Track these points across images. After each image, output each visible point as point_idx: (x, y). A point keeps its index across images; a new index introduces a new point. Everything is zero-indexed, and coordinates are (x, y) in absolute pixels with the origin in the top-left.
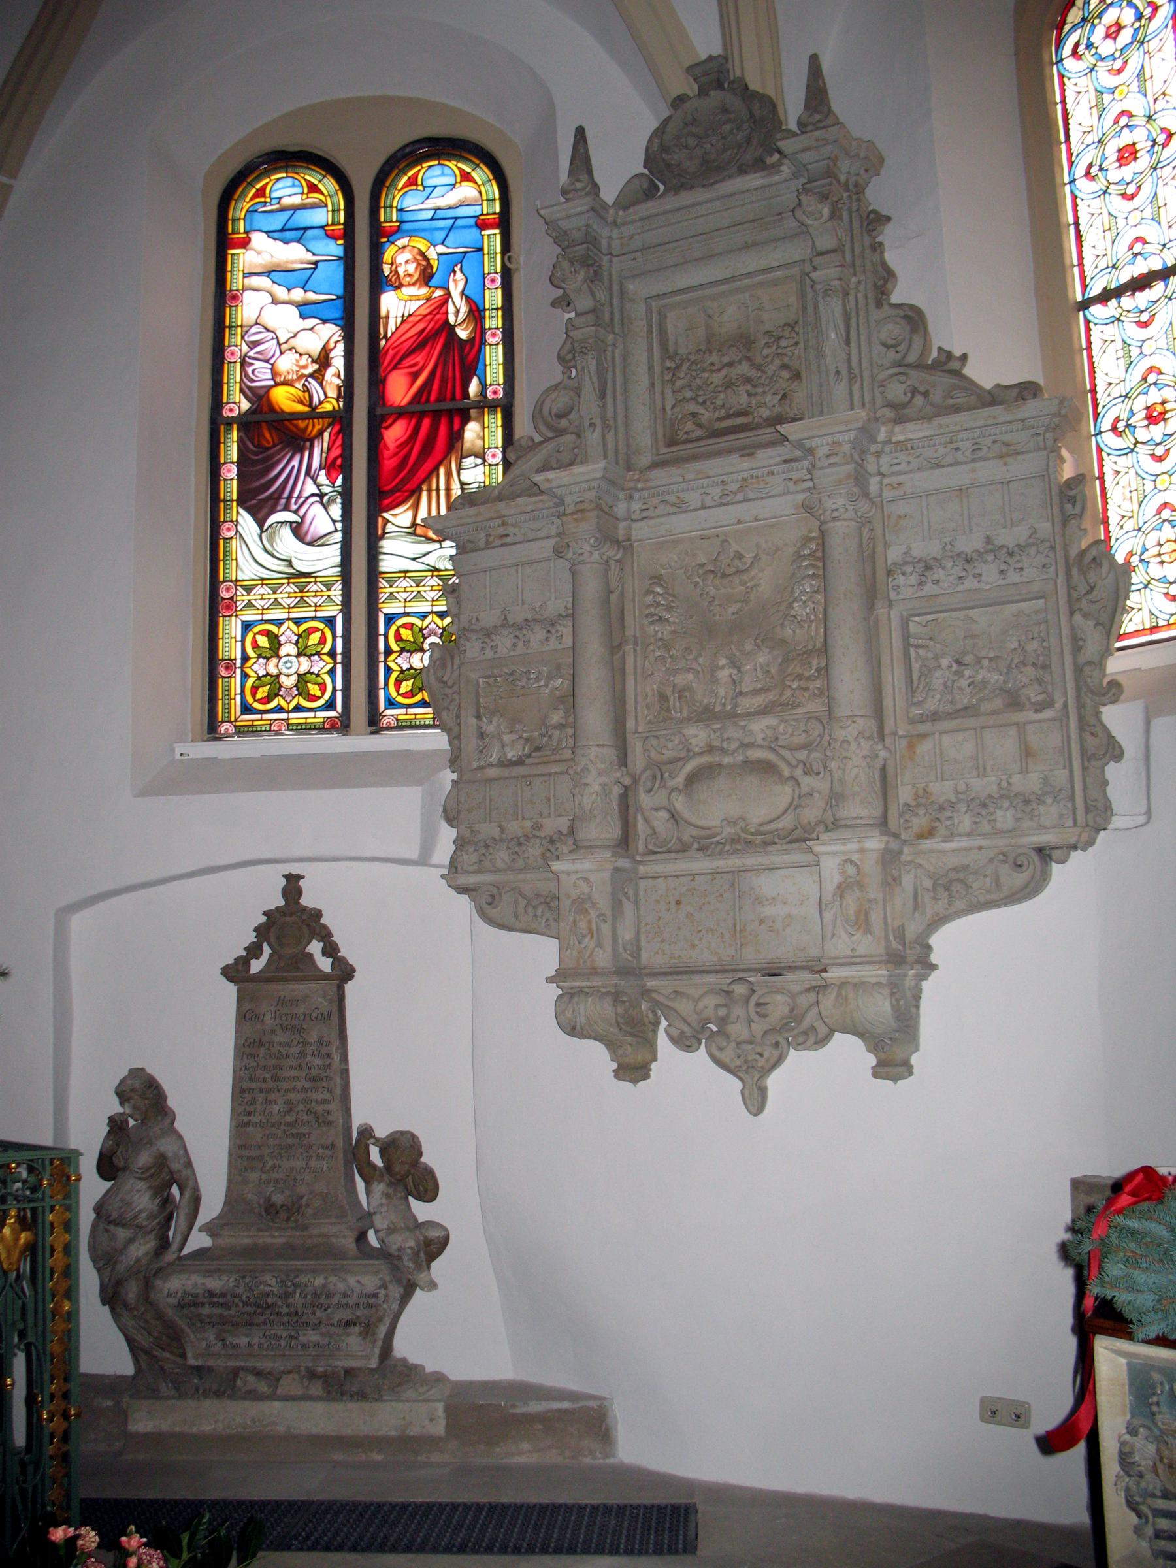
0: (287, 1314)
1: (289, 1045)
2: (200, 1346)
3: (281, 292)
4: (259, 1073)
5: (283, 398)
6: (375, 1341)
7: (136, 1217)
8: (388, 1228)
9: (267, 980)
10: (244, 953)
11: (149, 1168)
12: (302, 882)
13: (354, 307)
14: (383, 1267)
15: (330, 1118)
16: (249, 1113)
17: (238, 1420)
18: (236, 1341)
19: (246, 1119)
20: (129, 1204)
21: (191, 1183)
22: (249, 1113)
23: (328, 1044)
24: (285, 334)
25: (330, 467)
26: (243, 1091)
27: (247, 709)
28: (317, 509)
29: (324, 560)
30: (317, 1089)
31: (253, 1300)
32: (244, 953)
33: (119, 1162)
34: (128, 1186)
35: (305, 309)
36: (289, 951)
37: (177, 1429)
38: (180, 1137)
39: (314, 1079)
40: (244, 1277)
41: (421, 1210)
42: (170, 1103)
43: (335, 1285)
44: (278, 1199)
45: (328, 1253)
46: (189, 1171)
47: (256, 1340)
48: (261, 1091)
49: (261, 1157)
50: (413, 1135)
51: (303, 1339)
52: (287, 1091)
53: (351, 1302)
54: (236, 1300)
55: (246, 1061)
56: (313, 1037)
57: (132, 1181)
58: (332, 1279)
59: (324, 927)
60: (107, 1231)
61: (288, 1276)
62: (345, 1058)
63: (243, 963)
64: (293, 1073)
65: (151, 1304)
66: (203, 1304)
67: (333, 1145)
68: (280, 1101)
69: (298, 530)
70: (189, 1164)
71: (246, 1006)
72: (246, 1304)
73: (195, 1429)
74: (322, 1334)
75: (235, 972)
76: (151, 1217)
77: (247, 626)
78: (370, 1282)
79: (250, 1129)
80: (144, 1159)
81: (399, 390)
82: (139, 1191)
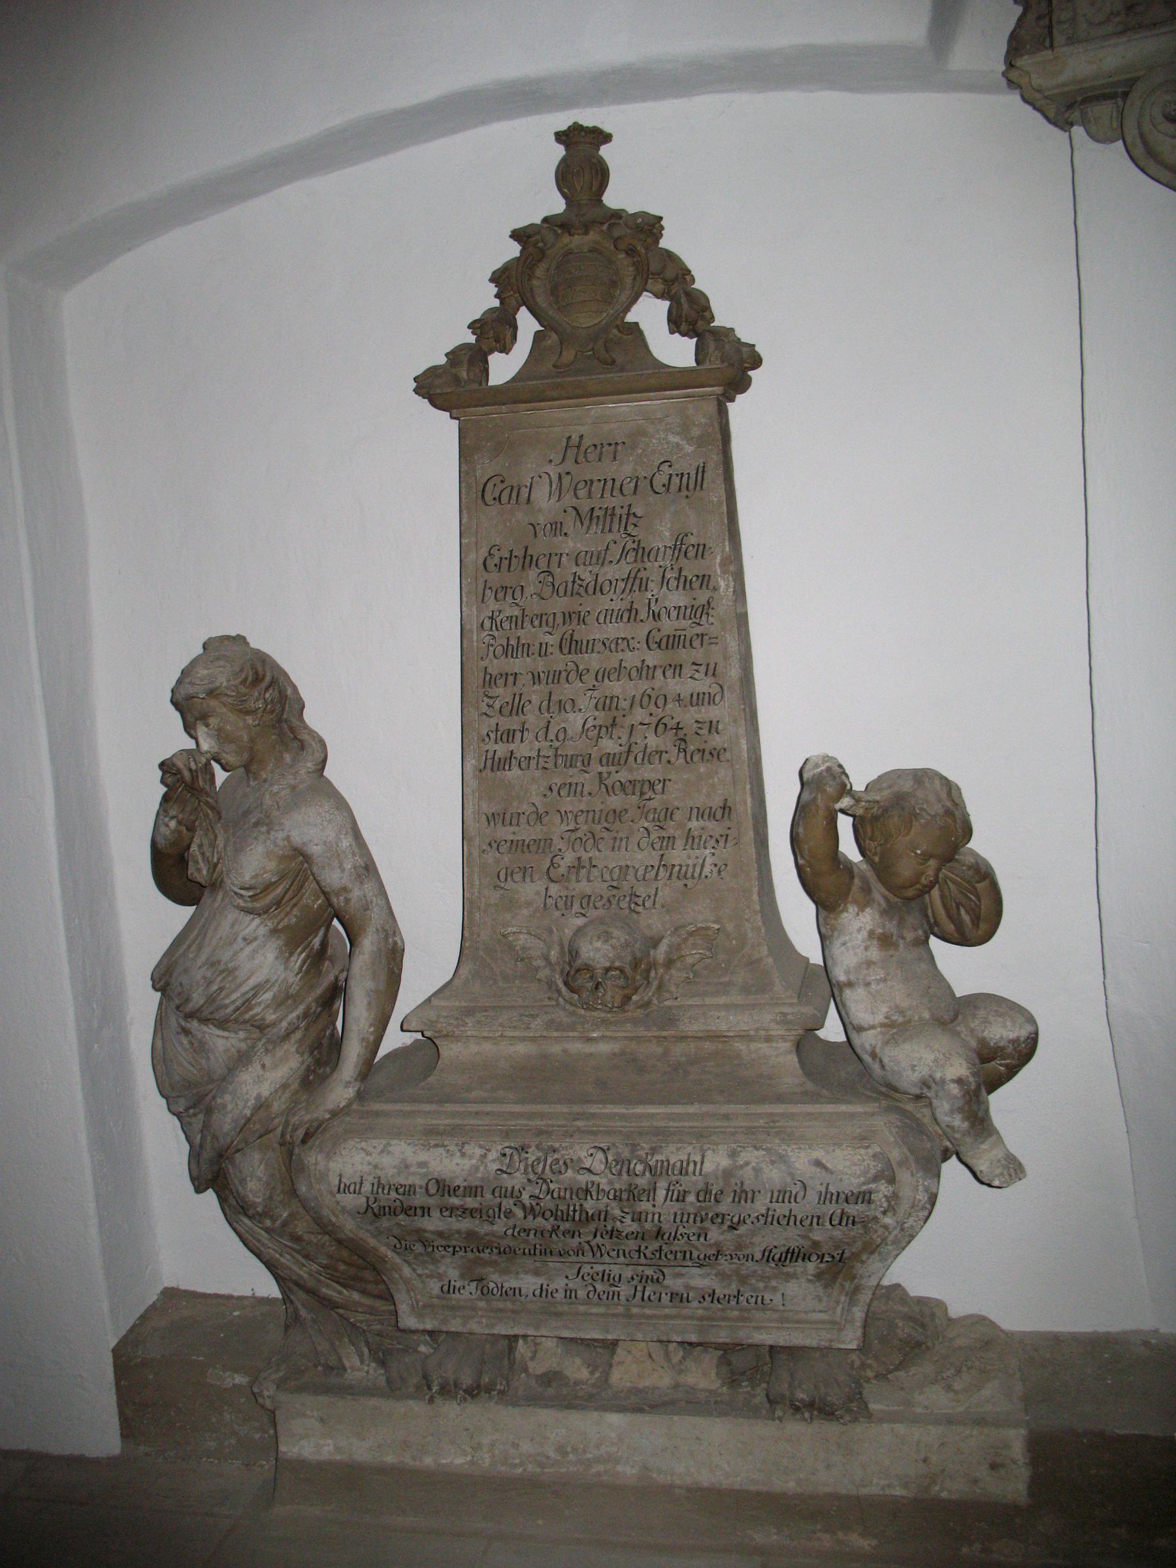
0: (636, 1236)
1: (600, 559)
2: (420, 1294)
4: (526, 634)
6: (857, 1290)
7: (247, 1004)
8: (889, 1025)
9: (536, 397)
10: (472, 339)
11: (268, 887)
12: (605, 151)
14: (879, 1122)
15: (717, 741)
16: (509, 736)
17: (526, 1447)
18: (511, 1283)
19: (501, 749)
20: (231, 972)
21: (376, 917)
22: (509, 736)
23: (701, 550)
26: (490, 680)
30: (678, 668)
31: (547, 1203)
32: (472, 339)
33: (199, 871)
34: (225, 928)
36: (585, 320)
37: (390, 1459)
38: (341, 805)
39: (672, 642)
40: (523, 1149)
41: (961, 967)
42: (312, 717)
43: (757, 1170)
44: (596, 952)
45: (725, 1079)
46: (369, 887)
47: (559, 1283)
48: (536, 678)
49: (549, 842)
50: (950, 788)
51: (673, 1283)
52: (603, 675)
53: (799, 1210)
54: (508, 1203)
55: (493, 605)
56: (662, 535)
57: (232, 915)
58: (750, 1156)
59: (670, 256)
60: (186, 1032)
61: (634, 1147)
62: (740, 593)
63: (471, 358)
64: (613, 630)
65: (304, 1204)
66: (426, 1211)
67: (726, 808)
68: (585, 702)
70: (369, 869)
71: (485, 468)
72: (530, 1211)
73: (428, 1461)
74: (723, 1276)
75: (450, 385)
76: (285, 999)
78: (848, 1166)
79: (514, 774)
80: (254, 862)
82: (248, 941)
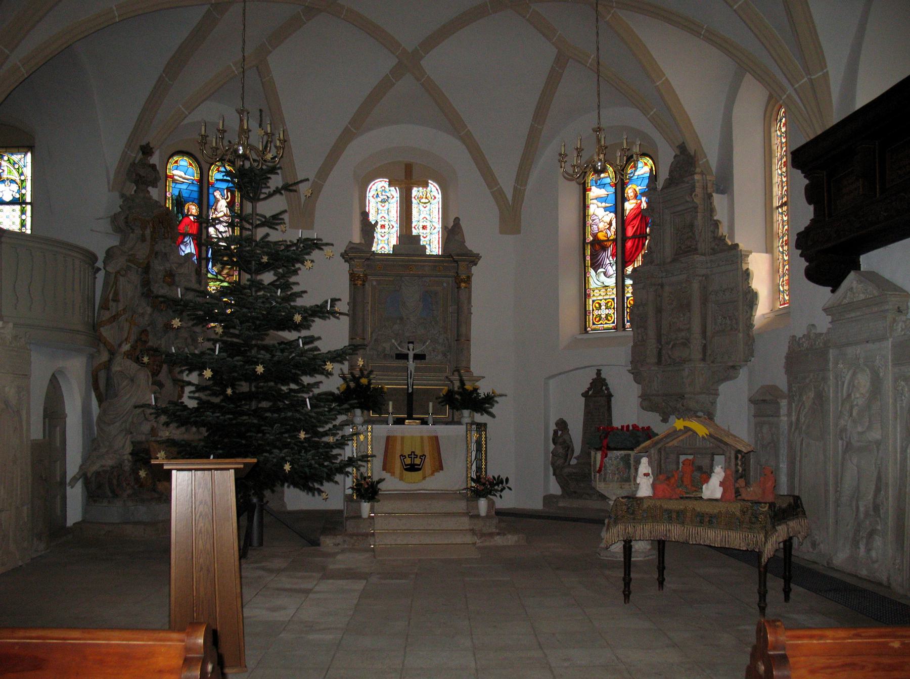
3: (599, 204)
5: (601, 236)
13: (618, 208)
24: (601, 218)
25: (612, 255)
27: (594, 324)
28: (610, 267)
29: (611, 282)
35: (606, 209)
63: (587, 392)
69: (605, 274)
75: (585, 395)
77: (593, 301)
81: (630, 232)
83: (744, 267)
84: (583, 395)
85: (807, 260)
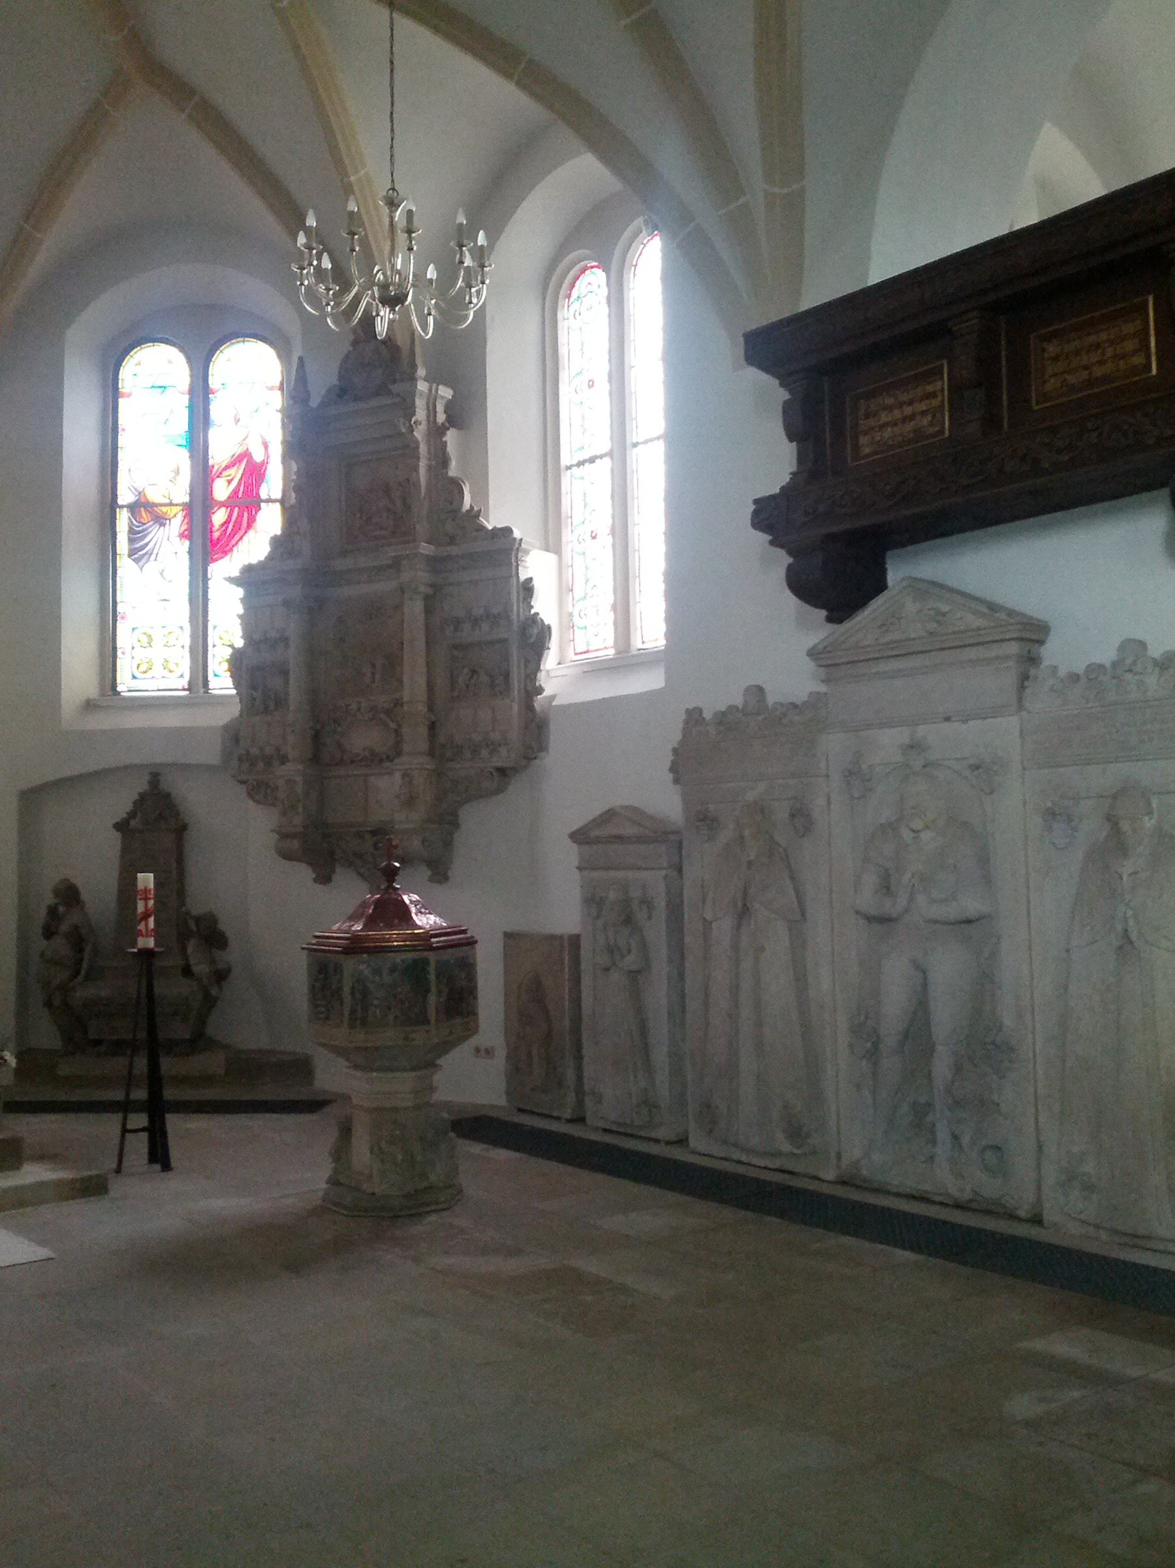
75: (121, 826)
81: (221, 490)
83: (523, 577)
84: (118, 826)
85: (790, 553)
